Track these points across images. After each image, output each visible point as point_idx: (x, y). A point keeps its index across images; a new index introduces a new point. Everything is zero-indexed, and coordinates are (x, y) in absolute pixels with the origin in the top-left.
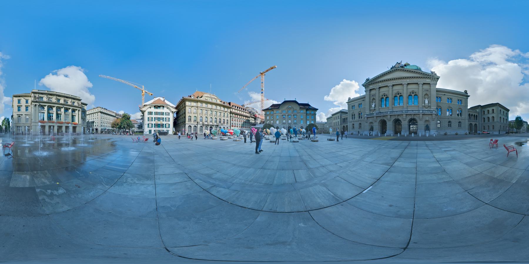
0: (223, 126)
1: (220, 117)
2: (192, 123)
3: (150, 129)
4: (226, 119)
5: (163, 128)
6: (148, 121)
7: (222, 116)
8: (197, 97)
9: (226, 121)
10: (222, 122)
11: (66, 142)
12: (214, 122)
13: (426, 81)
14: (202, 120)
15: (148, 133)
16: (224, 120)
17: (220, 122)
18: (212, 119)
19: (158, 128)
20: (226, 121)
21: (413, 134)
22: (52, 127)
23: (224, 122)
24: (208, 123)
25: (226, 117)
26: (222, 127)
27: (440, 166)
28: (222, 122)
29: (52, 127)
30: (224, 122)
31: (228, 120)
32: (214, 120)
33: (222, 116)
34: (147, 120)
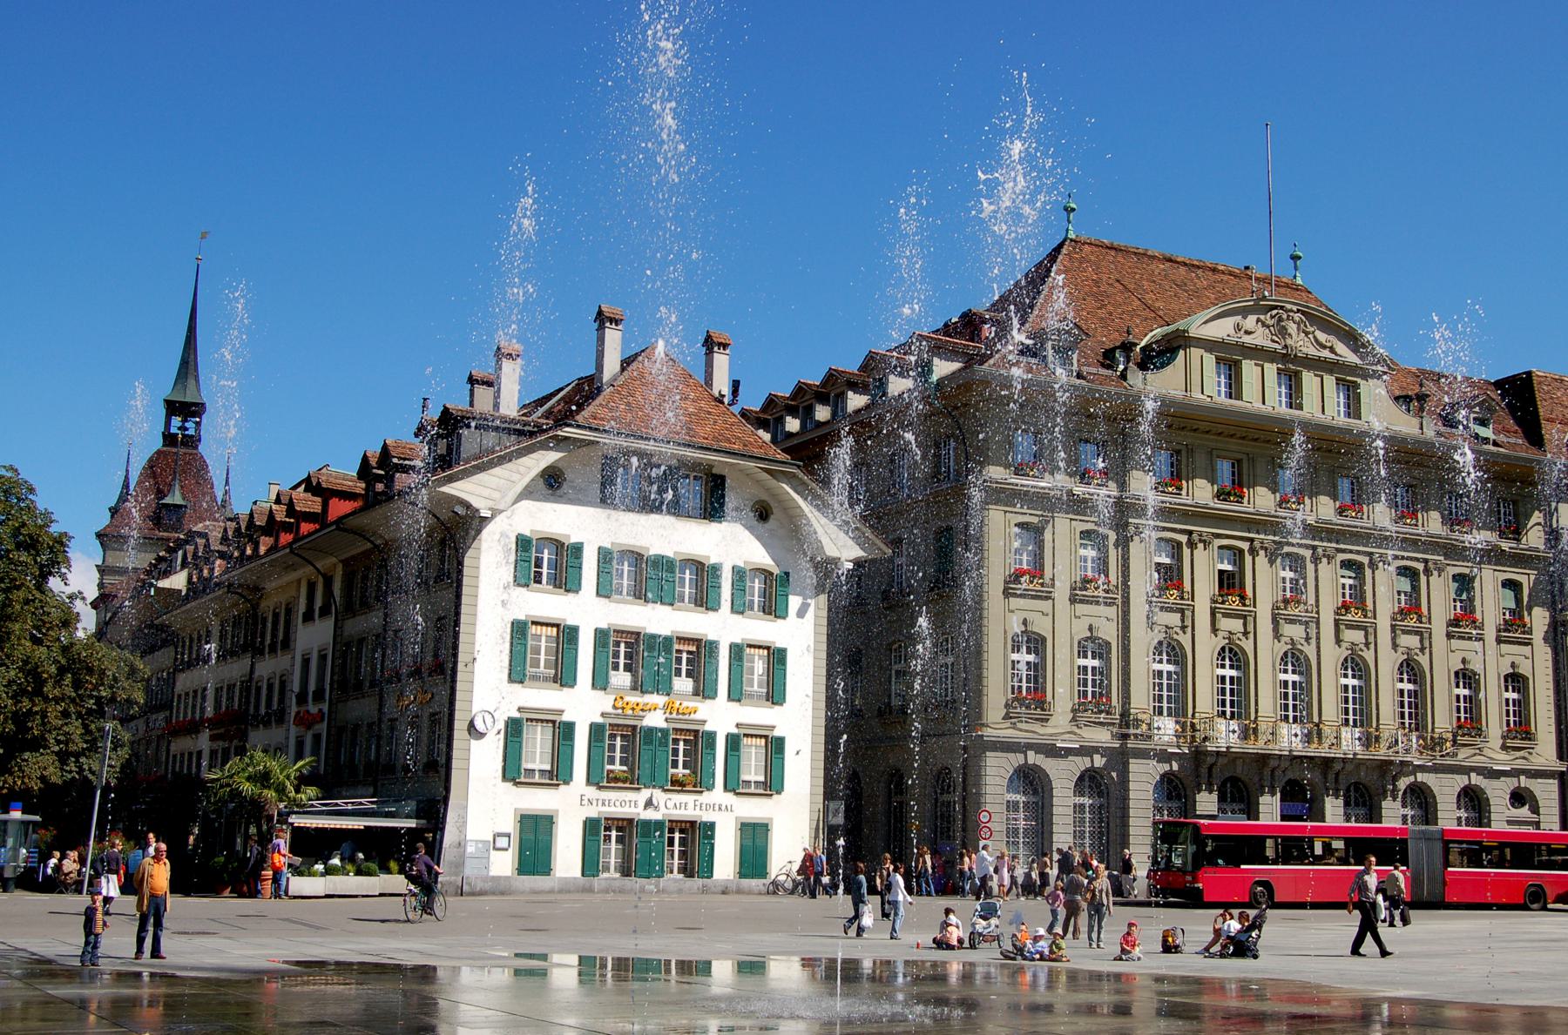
0: (1461, 781)
1: (1226, 624)
2: (1059, 725)
3: (538, 800)
4: (1492, 661)
5: (706, 797)
6: (517, 675)
7: (1439, 627)
8: (1108, 359)
9: (1495, 701)
10: (1443, 720)
11: (1223, 385)
12: (1205, 699)
13: (727, 578)
14: (1177, 699)
15: (503, 864)
16: (1036, 643)
17: (1416, 710)
18: (1306, 673)
19: (645, 794)
20: (1495, 701)
21: (1031, 658)
22: (1414, 522)
23: (1470, 723)
24: (1314, 734)
25: (1490, 633)
26: (1445, 789)
27: (369, 545)
28: (1443, 720)
29: (1414, 522)
30: (1470, 723)
31: (1515, 680)
32: (1332, 684)
33: (1439, 627)
34: (522, 705)
